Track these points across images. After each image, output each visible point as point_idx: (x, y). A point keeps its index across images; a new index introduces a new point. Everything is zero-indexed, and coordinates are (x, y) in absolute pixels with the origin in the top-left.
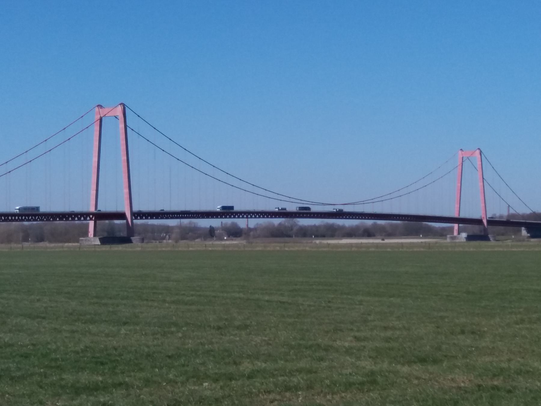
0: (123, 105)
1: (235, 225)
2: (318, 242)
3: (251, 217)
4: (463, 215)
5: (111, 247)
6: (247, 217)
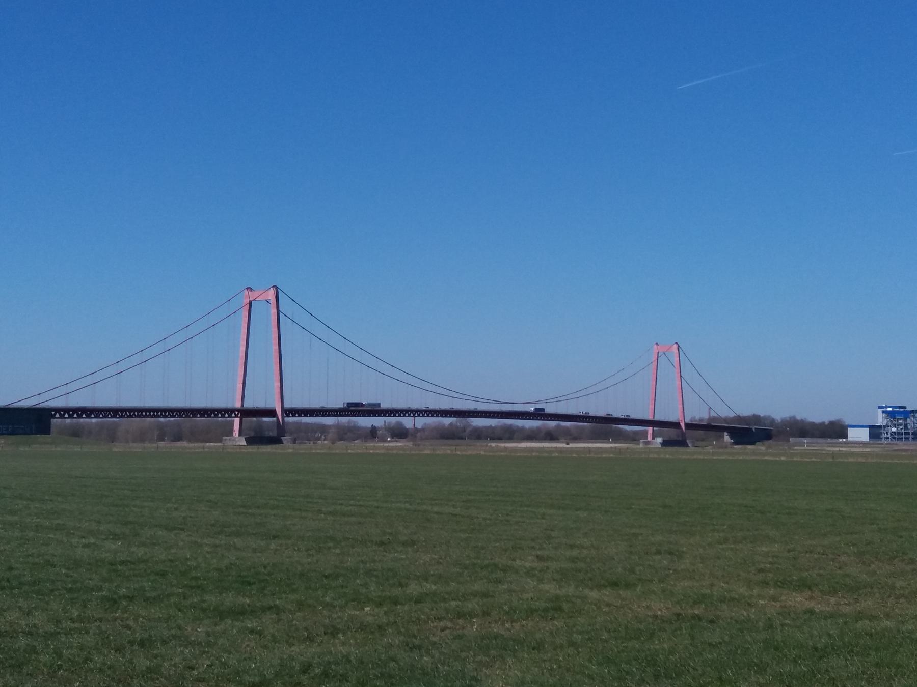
0: (276, 288)
1: (400, 425)
2: (493, 445)
3: (419, 416)
4: (658, 418)
5: (258, 448)
6: (414, 416)
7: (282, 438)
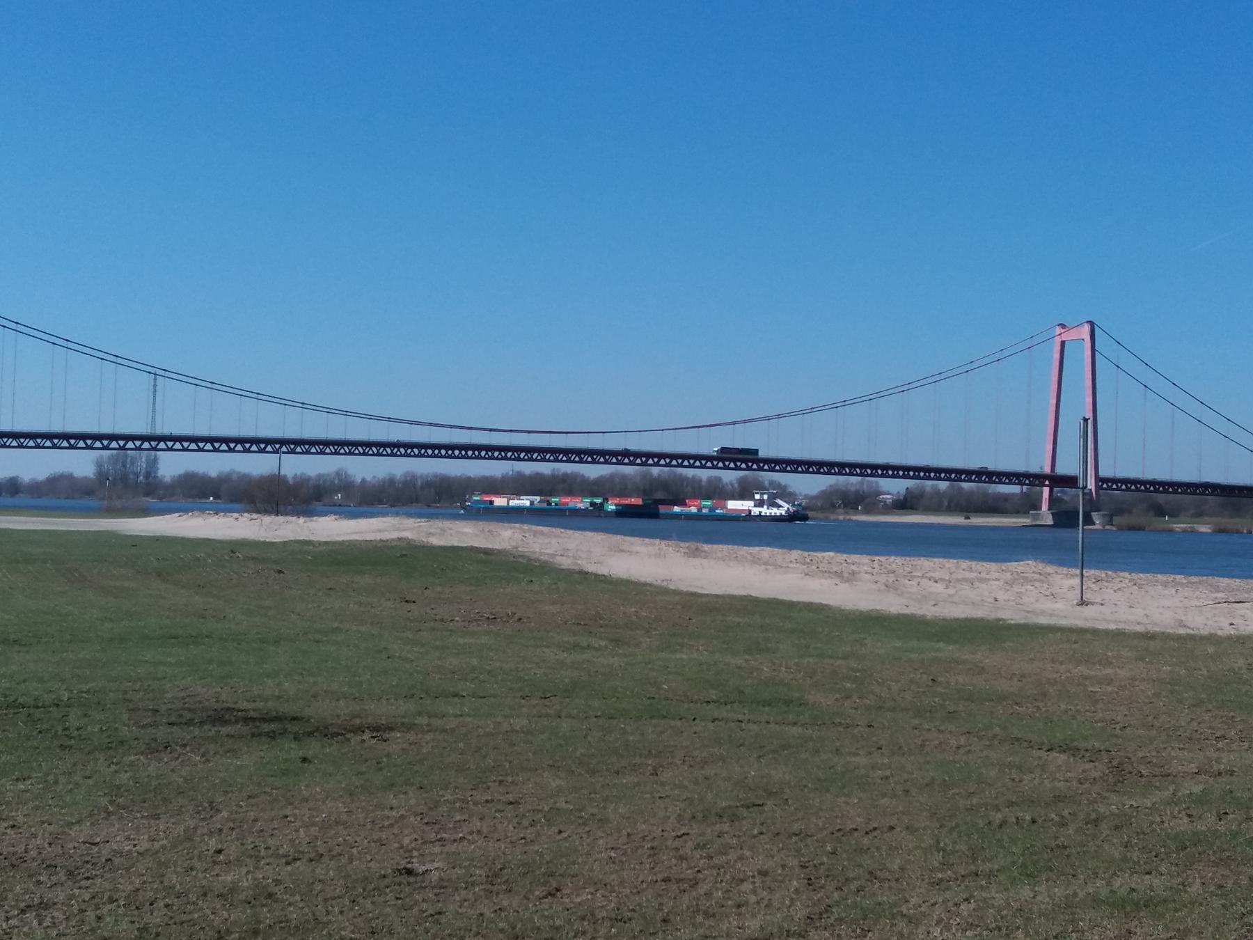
0: (1092, 324)
4: (159, 431)
7: (660, 506)
